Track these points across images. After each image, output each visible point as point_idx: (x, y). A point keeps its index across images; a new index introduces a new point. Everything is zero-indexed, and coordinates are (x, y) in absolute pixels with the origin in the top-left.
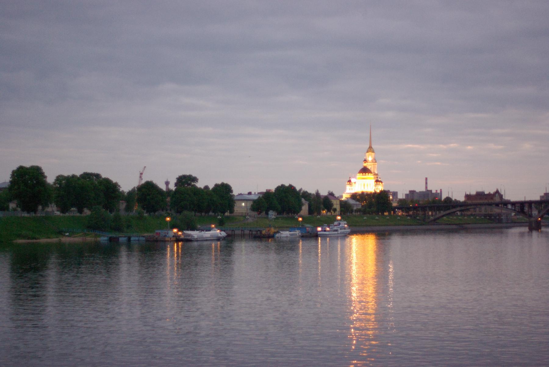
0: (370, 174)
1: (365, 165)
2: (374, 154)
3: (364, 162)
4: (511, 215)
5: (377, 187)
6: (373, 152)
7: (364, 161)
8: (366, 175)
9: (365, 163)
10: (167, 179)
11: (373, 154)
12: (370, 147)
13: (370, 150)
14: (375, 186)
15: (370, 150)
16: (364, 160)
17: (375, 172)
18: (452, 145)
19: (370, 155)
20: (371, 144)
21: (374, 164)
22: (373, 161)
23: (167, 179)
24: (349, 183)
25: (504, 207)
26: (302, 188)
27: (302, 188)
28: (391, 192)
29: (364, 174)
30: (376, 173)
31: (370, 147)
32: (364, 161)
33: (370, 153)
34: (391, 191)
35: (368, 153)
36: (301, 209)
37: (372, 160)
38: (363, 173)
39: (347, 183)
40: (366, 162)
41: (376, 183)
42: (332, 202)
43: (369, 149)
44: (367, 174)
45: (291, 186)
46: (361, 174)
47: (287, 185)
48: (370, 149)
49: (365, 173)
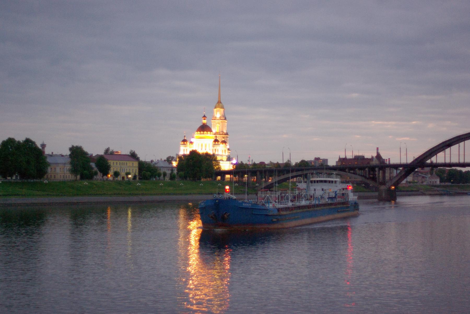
0: (209, 133)
1: (205, 121)
2: (223, 109)
3: (203, 118)
4: (110, 181)
5: (215, 148)
6: (222, 107)
7: (203, 117)
8: (204, 134)
9: (204, 119)
10: (43, 142)
11: (222, 110)
12: (219, 102)
13: (219, 105)
14: (213, 147)
15: (219, 105)
16: (203, 116)
17: (223, 131)
18: (414, 122)
19: (218, 111)
20: (220, 99)
21: (222, 122)
22: (222, 118)
23: (43, 142)
24: (183, 143)
25: (349, 172)
26: (109, 148)
27: (109, 148)
28: (321, 159)
29: (202, 132)
30: (225, 132)
31: (219, 102)
32: (203, 117)
33: (218, 109)
34: (321, 158)
35: (216, 109)
36: (114, 173)
37: (220, 117)
38: (200, 132)
39: (181, 143)
40: (205, 118)
41: (214, 143)
42: (109, 164)
43: (218, 104)
44: (205, 132)
45: (28, 141)
46: (199, 132)
47: (191, 150)
48: (219, 104)
49: (203, 131)
